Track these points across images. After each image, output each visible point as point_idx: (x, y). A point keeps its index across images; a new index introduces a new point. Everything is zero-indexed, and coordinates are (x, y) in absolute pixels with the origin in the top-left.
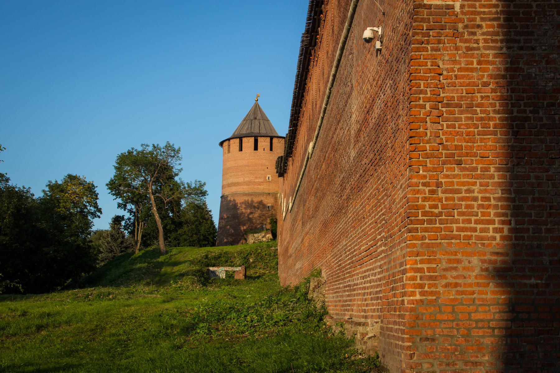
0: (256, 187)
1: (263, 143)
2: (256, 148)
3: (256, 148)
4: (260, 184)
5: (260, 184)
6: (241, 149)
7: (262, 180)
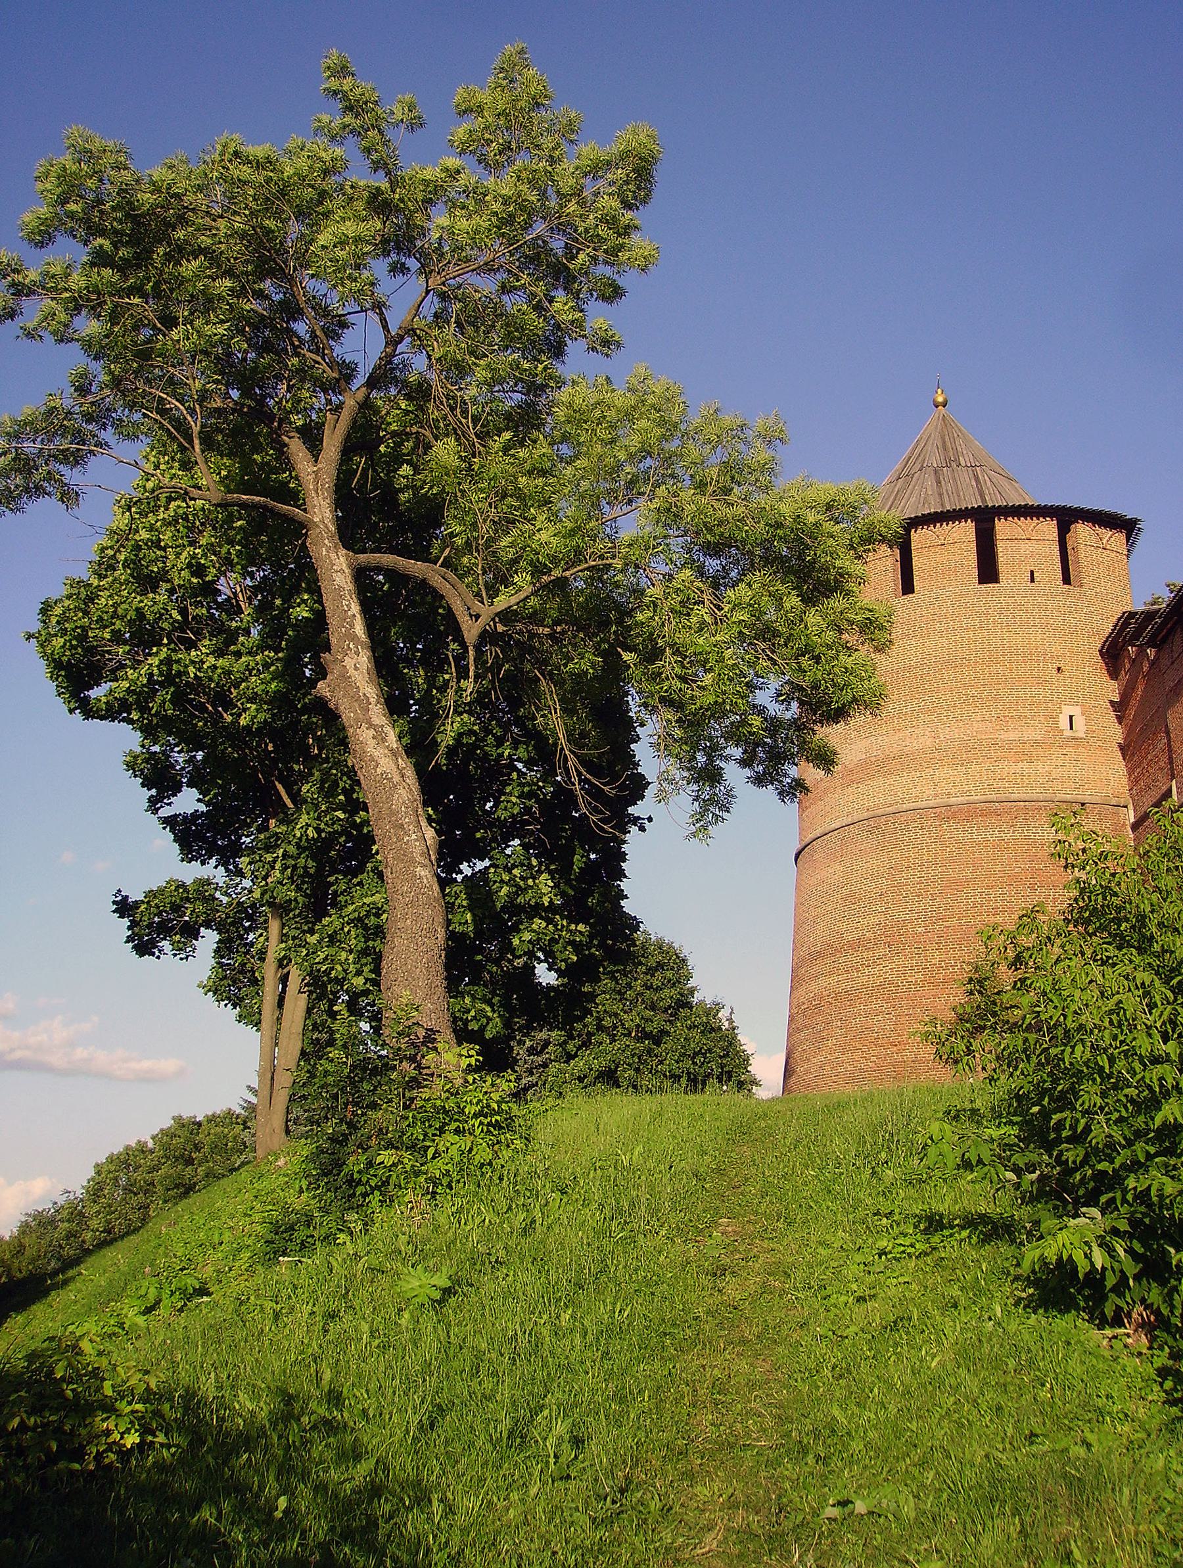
0: (1008, 768)
1: (1026, 548)
2: (988, 571)
3: (988, 571)
4: (1025, 752)
5: (1025, 752)
6: (908, 587)
7: (1033, 734)
